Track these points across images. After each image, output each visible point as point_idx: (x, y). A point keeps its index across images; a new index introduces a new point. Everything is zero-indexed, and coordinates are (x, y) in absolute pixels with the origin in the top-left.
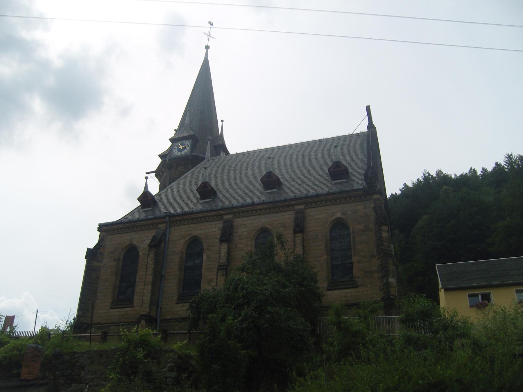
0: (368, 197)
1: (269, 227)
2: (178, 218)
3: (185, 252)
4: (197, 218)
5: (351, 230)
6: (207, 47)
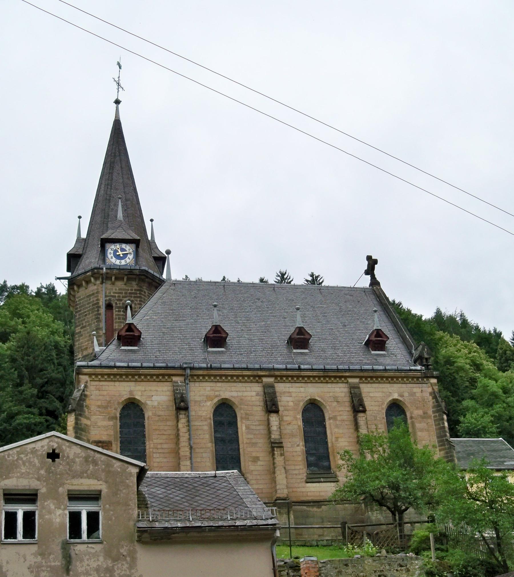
0: (425, 380)
1: (317, 398)
2: (200, 372)
4: (226, 376)
5: (408, 414)
6: (117, 102)
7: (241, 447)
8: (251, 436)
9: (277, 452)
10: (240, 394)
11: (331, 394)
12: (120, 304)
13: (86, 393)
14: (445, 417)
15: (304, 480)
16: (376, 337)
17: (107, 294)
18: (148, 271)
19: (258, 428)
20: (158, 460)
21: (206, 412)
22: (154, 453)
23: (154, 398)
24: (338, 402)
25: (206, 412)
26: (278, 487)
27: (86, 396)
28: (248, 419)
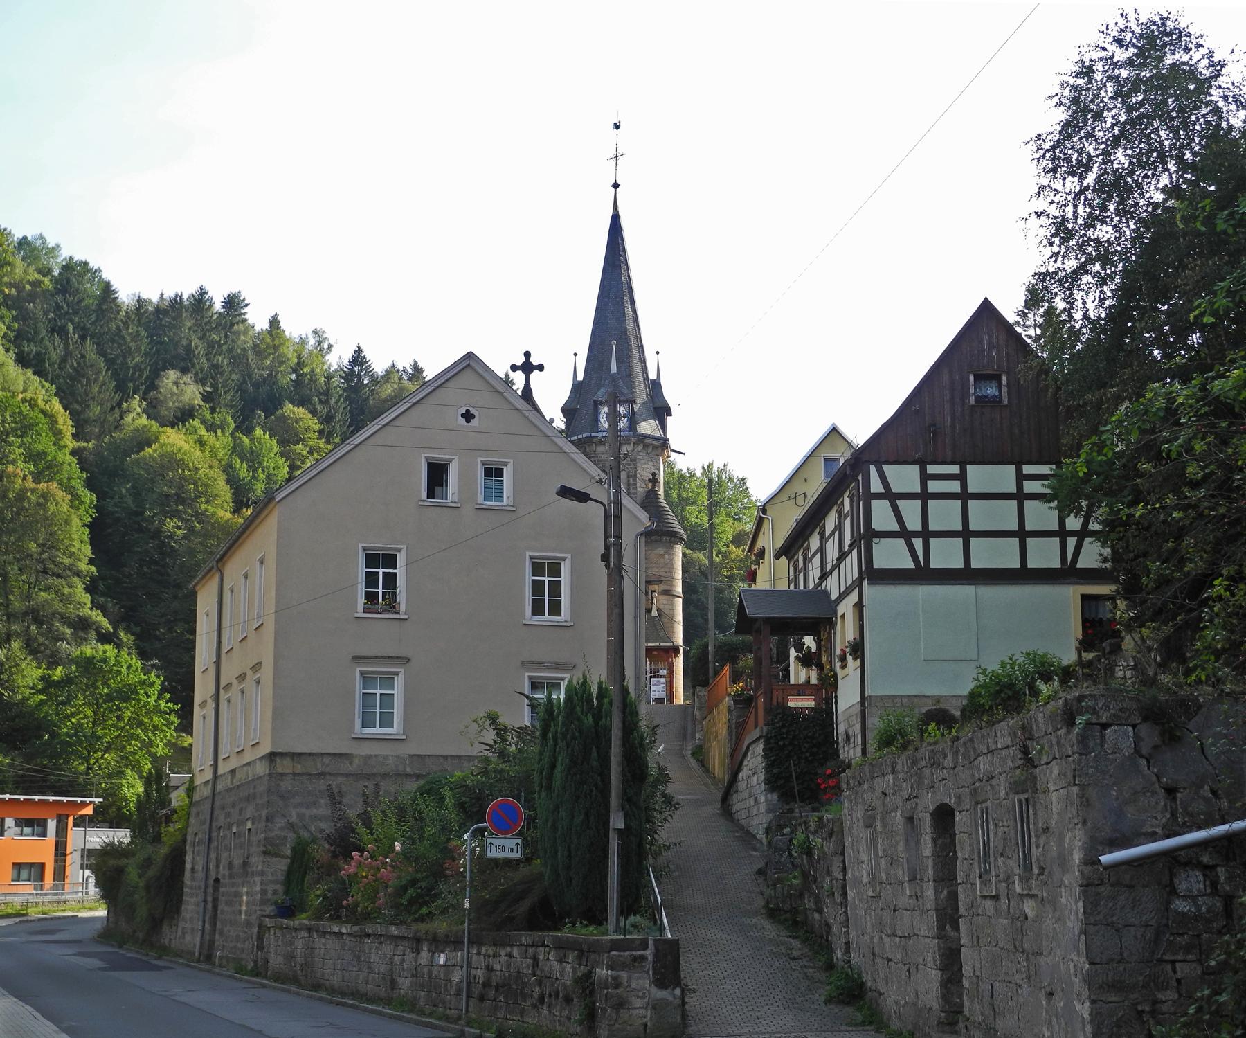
6: (616, 186)
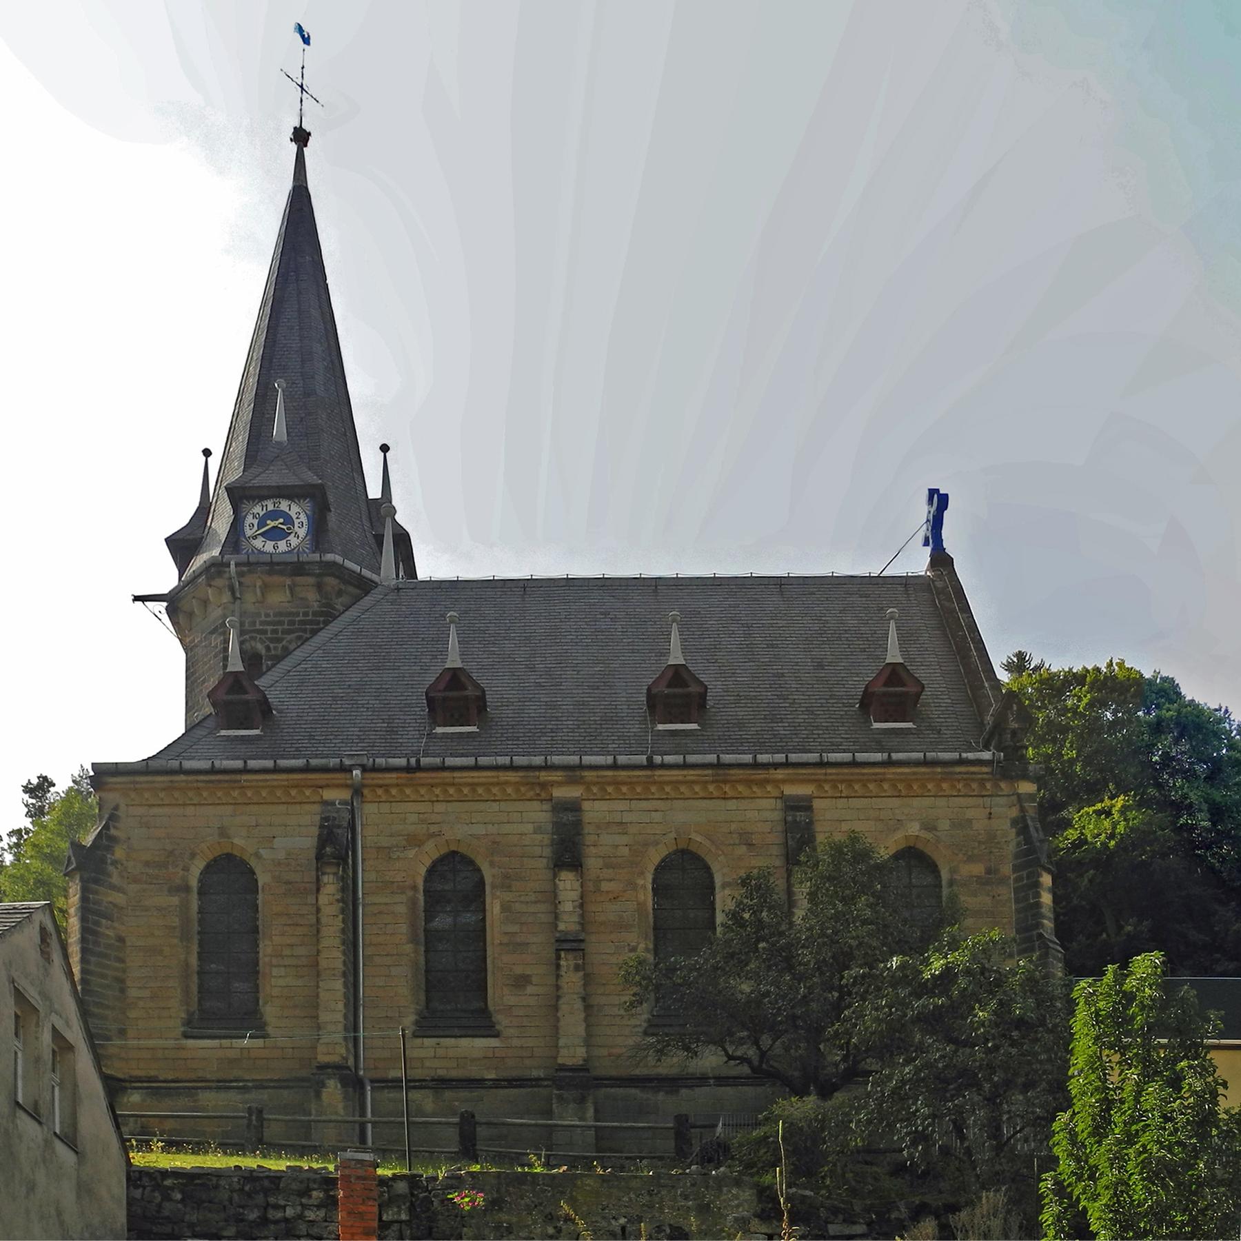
3: (421, 888)
5: (945, 875)
6: (301, 137)
7: (489, 953)
8: (516, 928)
9: (567, 962)
10: (492, 829)
11: (733, 826)
12: (275, 648)
13: (113, 832)
14: (1046, 879)
15: (641, 1030)
16: (886, 684)
17: (247, 627)
18: (342, 566)
19: (532, 909)
20: (281, 982)
21: (404, 874)
22: (272, 966)
23: (278, 842)
24: (750, 845)
25: (404, 874)
26: (562, 1042)
27: (114, 840)
28: (509, 888)
